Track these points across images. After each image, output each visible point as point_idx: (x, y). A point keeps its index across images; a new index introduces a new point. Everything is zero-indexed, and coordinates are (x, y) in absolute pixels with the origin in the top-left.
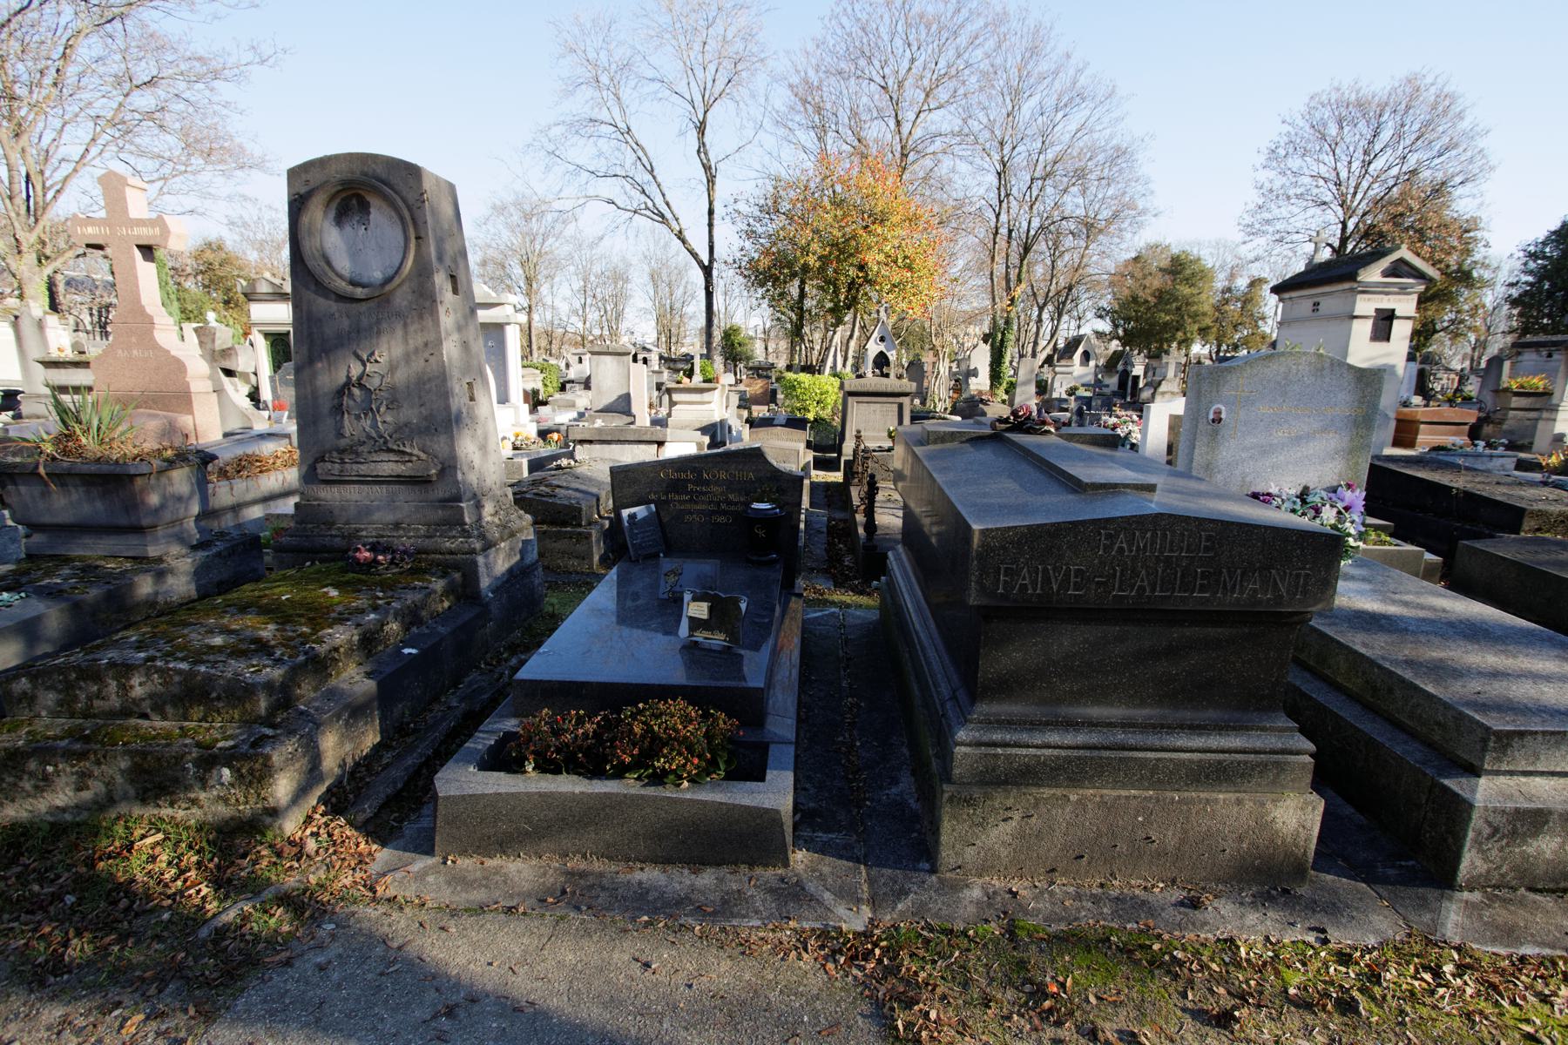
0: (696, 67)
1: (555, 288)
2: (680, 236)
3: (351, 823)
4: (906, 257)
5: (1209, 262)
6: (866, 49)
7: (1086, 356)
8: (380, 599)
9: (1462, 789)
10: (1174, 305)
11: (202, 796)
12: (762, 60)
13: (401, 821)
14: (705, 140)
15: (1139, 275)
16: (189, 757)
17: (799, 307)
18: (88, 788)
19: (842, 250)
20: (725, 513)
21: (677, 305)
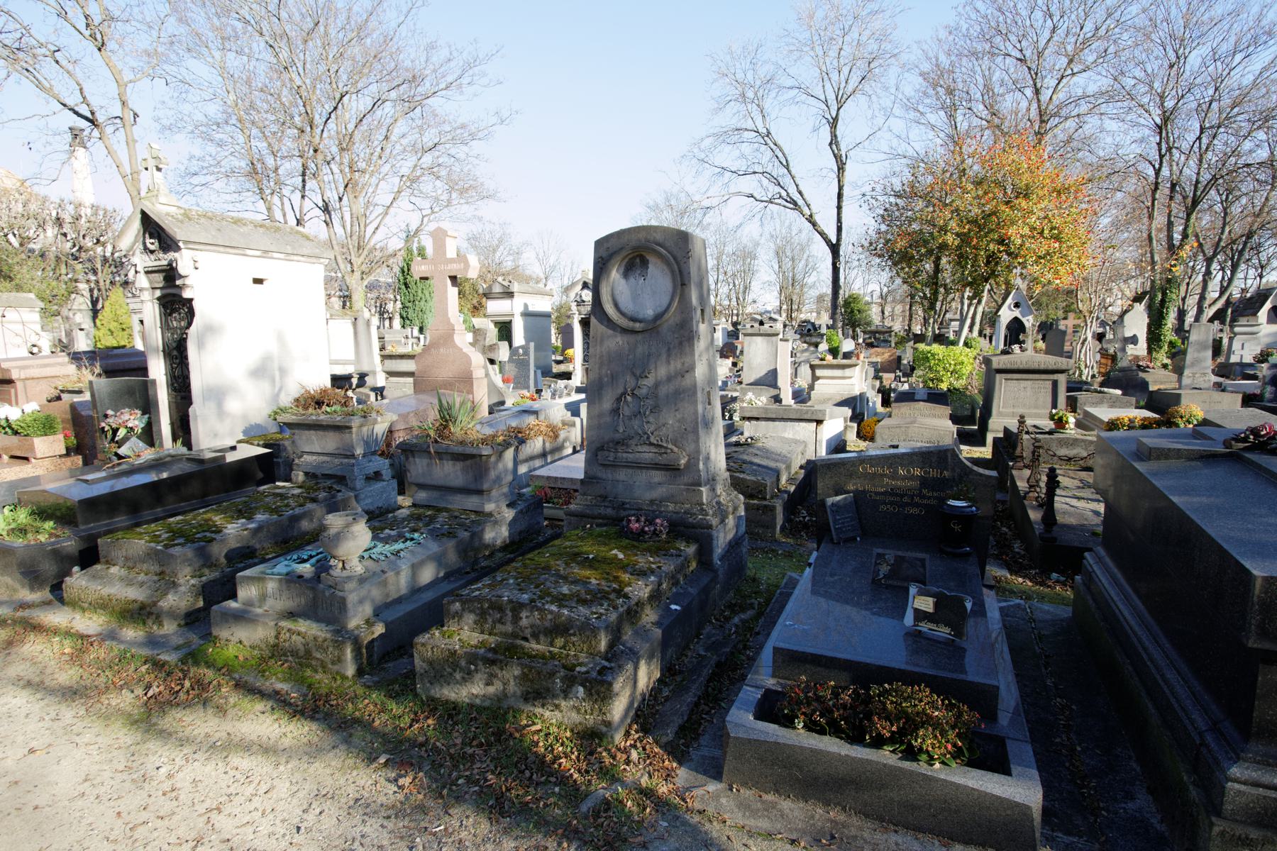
2: (811, 220)
3: (656, 742)
4: (1052, 229)
11: (563, 703)
12: (895, 55)
13: (688, 747)
14: (838, 133)
16: (558, 675)
17: (934, 281)
18: (493, 684)
19: (982, 224)
20: (917, 505)
21: (799, 277)
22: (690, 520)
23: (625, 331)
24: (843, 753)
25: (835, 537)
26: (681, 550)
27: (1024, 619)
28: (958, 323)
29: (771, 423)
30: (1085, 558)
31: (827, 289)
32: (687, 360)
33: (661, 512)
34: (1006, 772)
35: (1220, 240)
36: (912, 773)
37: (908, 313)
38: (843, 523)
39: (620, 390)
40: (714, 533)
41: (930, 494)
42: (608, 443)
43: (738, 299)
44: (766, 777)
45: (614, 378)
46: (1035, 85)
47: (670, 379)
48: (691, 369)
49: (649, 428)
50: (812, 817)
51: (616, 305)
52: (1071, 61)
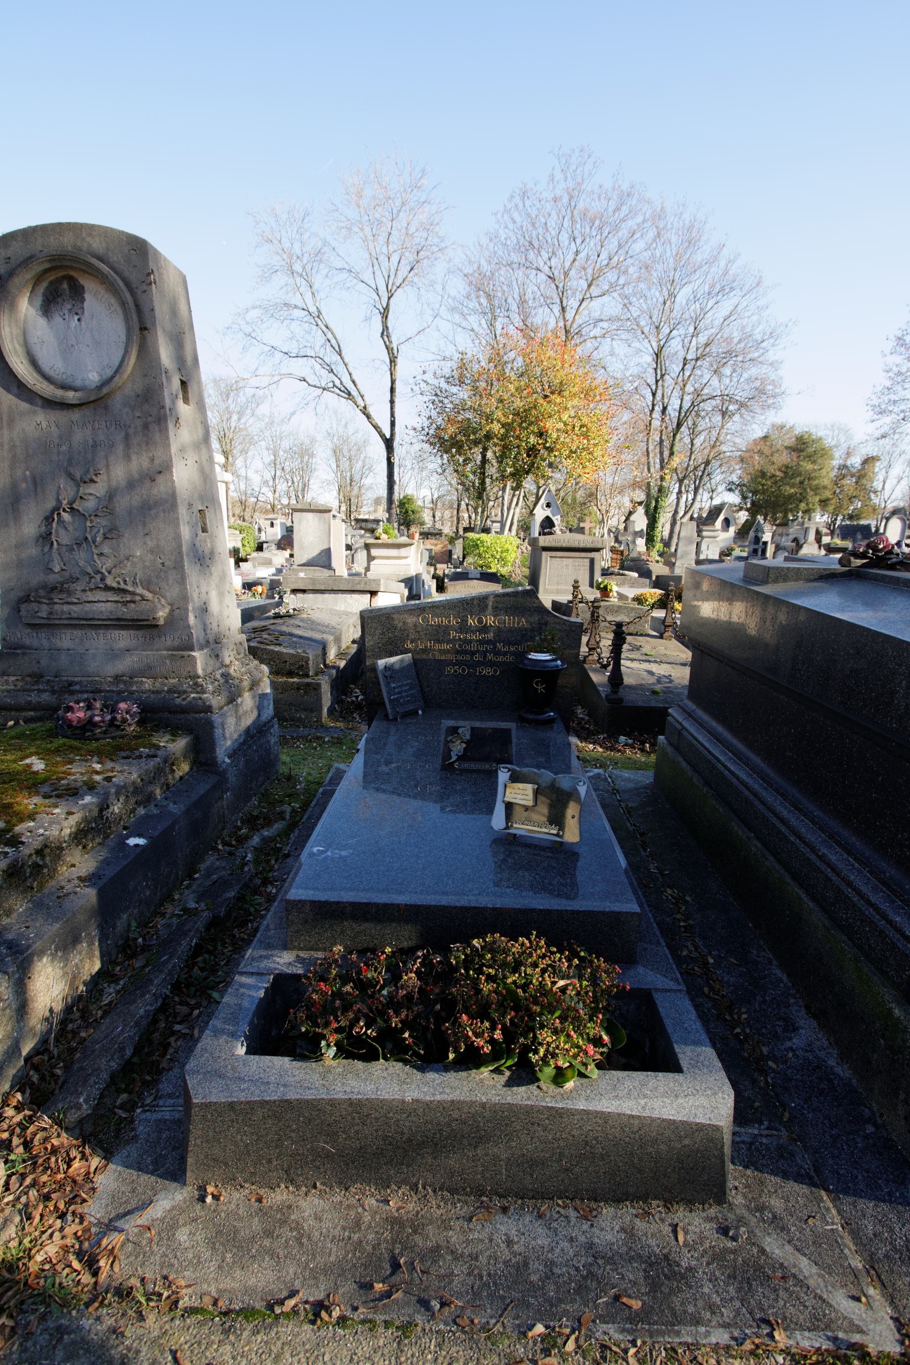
0: (381, 258)
1: (248, 462)
4: (581, 426)
5: (829, 442)
6: (536, 244)
7: (727, 523)
8: (97, 773)
9: (269, 704)
10: (798, 479)
14: (389, 324)
15: (767, 451)
19: (524, 417)
20: (491, 664)
21: (356, 477)
22: (178, 701)
23: (50, 404)
24: (408, 1099)
25: (389, 711)
26: (158, 747)
27: (607, 792)
28: (499, 525)
29: (319, 596)
30: (669, 715)
31: (384, 493)
32: (159, 453)
33: (132, 693)
34: (670, 1065)
35: (688, 465)
36: (529, 1111)
37: (455, 518)
38: (399, 693)
39: (50, 504)
40: (216, 718)
41: (506, 649)
42: (36, 590)
43: (297, 497)
44: (270, 1161)
45: (37, 483)
46: (562, 302)
47: (131, 485)
48: (165, 468)
49: (104, 565)
50: (358, 1224)
51: (34, 363)
52: (589, 286)
